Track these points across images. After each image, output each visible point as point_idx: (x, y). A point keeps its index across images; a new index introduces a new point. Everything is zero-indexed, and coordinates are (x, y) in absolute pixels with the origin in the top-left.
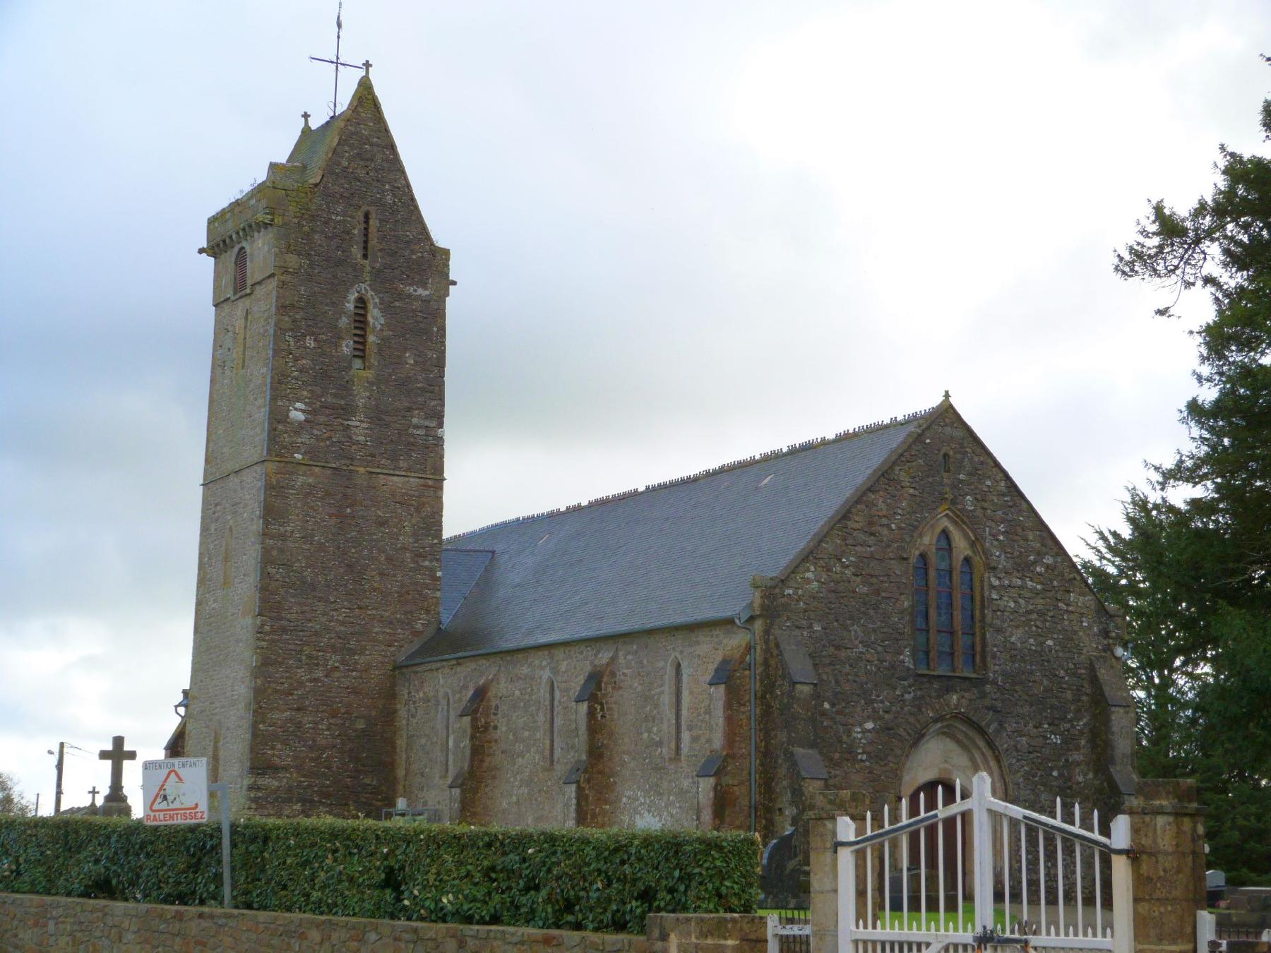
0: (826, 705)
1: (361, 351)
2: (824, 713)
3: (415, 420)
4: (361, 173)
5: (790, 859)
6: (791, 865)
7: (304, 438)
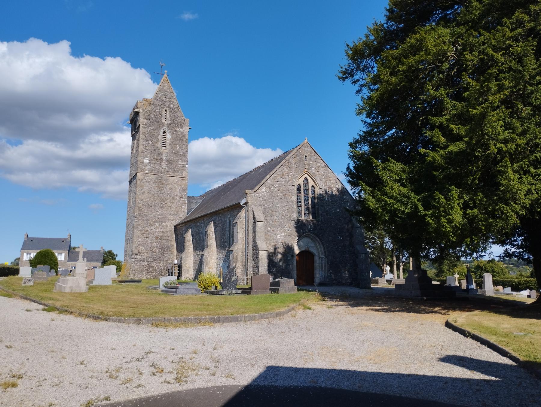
0: (269, 229)
1: (164, 145)
2: (268, 231)
3: (180, 163)
4: (164, 99)
5: (233, 276)
6: (234, 278)
7: (149, 167)
